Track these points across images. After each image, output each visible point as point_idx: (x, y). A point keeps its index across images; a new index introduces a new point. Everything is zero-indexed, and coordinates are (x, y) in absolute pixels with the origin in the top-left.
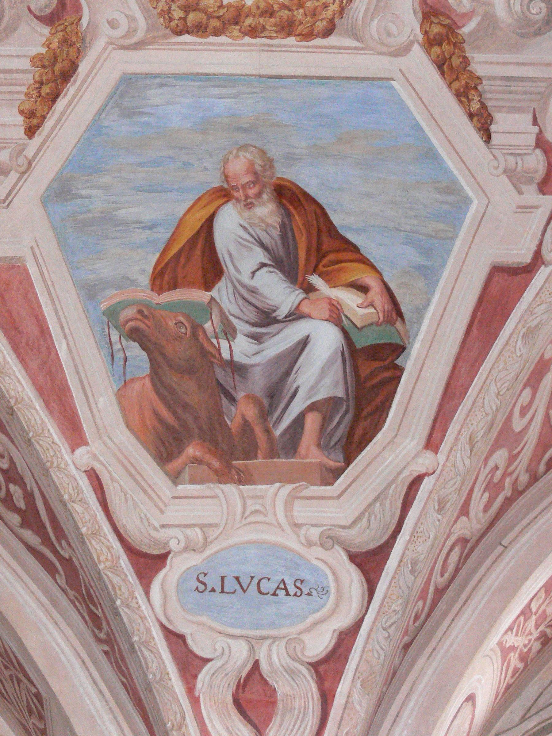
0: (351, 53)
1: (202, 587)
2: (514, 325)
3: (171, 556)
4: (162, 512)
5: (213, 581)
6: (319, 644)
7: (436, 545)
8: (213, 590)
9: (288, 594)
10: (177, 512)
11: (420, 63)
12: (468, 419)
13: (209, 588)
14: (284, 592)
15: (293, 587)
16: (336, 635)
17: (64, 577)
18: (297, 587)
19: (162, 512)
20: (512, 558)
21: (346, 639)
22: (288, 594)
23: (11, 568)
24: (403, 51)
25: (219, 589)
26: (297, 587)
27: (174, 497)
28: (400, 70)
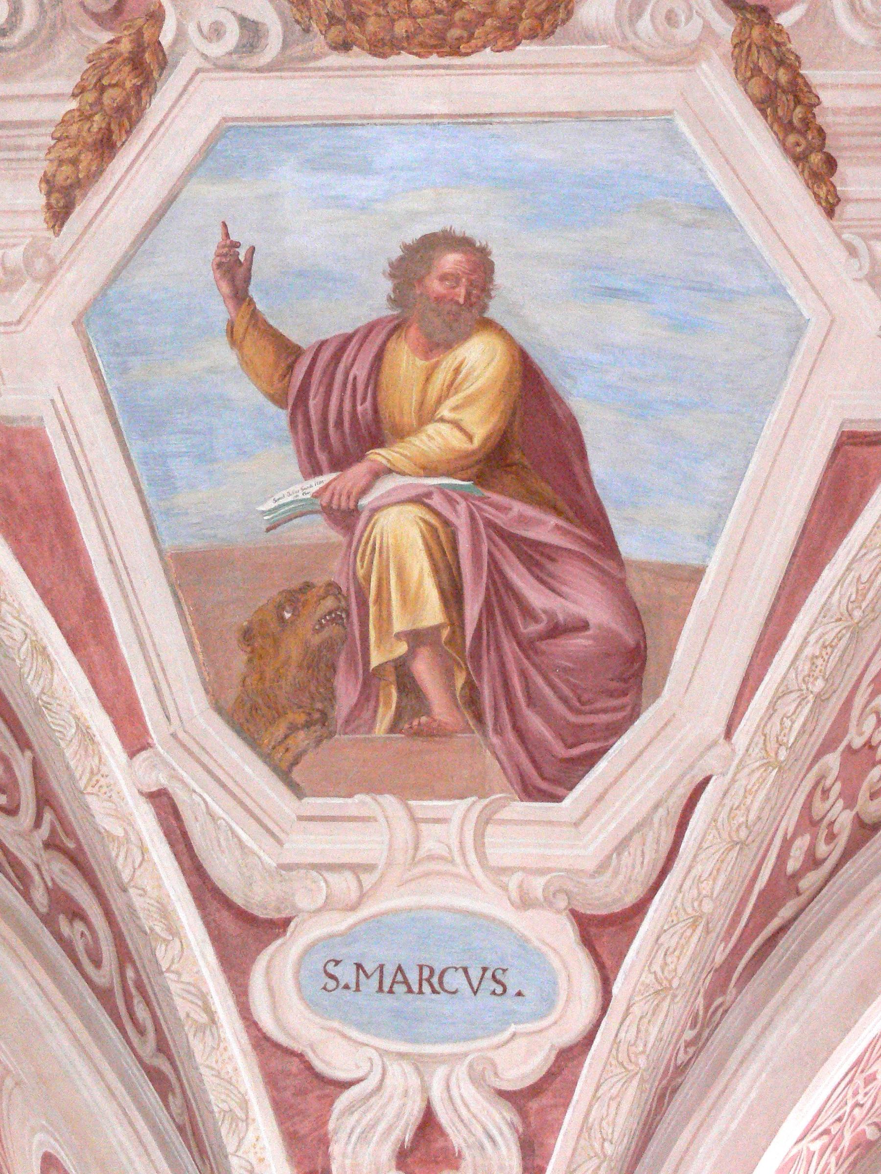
0: (136, 597)
1: (332, 984)
2: (793, 655)
3: (292, 924)
4: (280, 842)
5: (346, 973)
6: (522, 1066)
7: (791, 940)
8: (346, 987)
9: (410, 991)
10: (309, 844)
11: (721, 93)
12: (387, 842)
13: (342, 984)
14: (404, 988)
15: (339, 979)
16: (554, 1053)
17: (728, 951)
18: (332, 977)
19: (280, 842)
20: (837, 966)
21: (570, 1057)
22: (410, 991)
23: (505, 67)
24: (686, 57)
25: (353, 986)
26: (332, 977)
27: (300, 818)
28: (268, 530)
